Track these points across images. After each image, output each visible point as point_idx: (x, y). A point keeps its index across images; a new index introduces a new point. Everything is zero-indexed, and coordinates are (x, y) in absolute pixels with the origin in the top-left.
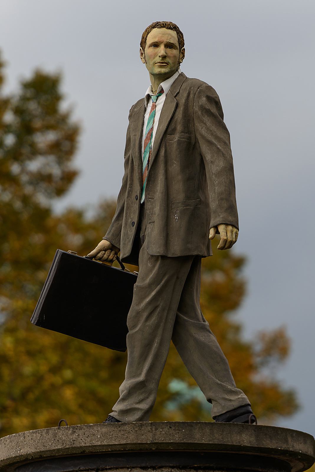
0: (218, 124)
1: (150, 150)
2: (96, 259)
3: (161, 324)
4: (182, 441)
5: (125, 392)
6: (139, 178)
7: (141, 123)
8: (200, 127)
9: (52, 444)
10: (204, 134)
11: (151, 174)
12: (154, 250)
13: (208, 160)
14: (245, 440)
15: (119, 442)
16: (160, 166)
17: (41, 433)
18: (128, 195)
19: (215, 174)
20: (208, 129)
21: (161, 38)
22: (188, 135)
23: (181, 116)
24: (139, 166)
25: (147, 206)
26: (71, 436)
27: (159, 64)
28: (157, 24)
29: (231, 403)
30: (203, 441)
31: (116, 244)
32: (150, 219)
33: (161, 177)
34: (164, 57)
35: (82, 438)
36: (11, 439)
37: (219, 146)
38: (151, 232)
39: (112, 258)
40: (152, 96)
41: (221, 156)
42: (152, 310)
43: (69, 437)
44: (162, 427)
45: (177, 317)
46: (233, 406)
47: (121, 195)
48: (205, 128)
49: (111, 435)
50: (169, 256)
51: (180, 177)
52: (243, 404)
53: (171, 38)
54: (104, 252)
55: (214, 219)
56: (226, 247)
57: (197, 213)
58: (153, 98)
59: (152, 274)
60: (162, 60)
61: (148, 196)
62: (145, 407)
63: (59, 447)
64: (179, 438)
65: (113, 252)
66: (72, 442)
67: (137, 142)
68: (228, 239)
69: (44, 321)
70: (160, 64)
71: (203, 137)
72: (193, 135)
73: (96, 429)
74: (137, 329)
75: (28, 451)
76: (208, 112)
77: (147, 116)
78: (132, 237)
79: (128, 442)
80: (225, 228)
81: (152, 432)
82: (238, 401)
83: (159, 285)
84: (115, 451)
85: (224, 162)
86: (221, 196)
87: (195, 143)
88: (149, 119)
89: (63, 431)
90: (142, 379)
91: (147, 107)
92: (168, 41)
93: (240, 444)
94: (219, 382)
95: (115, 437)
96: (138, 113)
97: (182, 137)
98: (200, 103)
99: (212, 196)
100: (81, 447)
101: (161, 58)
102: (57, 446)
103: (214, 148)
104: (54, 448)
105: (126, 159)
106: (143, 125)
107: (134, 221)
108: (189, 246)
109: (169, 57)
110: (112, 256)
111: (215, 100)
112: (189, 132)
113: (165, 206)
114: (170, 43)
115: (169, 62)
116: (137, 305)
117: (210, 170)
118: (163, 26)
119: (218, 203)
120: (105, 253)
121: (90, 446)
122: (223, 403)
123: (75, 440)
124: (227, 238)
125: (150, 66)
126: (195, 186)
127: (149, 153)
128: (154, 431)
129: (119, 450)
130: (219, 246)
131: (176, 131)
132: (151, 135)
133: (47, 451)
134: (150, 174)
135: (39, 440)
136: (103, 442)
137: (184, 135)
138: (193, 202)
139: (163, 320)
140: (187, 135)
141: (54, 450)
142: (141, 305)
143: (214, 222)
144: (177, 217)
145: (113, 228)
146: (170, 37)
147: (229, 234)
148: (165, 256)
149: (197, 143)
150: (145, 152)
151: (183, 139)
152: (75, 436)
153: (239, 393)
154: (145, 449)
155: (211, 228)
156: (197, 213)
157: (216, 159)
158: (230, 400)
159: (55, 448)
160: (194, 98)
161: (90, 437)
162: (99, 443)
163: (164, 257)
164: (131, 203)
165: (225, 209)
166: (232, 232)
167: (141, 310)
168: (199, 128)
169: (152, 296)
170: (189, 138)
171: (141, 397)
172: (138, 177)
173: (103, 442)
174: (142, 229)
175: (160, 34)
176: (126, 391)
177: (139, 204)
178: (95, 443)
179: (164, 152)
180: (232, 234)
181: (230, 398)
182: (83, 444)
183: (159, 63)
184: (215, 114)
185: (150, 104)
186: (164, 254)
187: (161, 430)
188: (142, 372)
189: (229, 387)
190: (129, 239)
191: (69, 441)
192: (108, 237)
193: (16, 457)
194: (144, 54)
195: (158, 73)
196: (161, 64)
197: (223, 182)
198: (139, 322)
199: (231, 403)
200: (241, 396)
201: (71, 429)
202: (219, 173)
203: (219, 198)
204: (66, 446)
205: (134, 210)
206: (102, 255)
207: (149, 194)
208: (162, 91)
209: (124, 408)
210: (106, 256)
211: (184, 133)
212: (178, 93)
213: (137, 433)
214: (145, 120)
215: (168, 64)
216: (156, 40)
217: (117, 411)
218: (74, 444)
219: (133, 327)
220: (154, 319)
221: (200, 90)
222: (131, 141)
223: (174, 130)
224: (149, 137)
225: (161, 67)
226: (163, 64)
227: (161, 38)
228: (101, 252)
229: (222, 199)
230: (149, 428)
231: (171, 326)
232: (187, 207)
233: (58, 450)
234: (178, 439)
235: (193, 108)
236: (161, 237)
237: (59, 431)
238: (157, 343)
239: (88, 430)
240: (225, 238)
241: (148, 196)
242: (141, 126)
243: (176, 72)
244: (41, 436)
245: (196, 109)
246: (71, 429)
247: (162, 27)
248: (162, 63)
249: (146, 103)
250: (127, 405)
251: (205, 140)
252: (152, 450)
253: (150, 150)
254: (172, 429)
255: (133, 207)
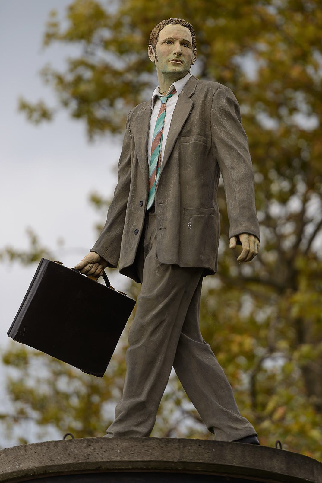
0: (238, 129)
1: (160, 152)
2: (82, 272)
3: (166, 341)
4: (212, 462)
5: (123, 412)
6: (146, 182)
7: (147, 126)
8: (219, 130)
9: (61, 459)
10: (224, 137)
11: (163, 177)
12: (166, 258)
13: (228, 165)
14: (276, 466)
15: (142, 459)
16: (172, 170)
17: (47, 446)
18: (131, 201)
19: (235, 180)
20: (227, 133)
21: (176, 35)
22: (205, 138)
23: (198, 118)
24: (146, 170)
25: (158, 211)
26: (85, 450)
27: (173, 62)
28: (172, 21)
29: (238, 432)
30: (235, 464)
31: (106, 257)
32: (161, 225)
33: (174, 181)
34: (180, 55)
35: (98, 452)
36: (7, 453)
37: (240, 152)
38: (162, 239)
39: (99, 272)
40: (161, 97)
41: (242, 162)
42: (158, 323)
43: (83, 450)
44: (191, 445)
45: (181, 337)
46: (240, 436)
47: (114, 205)
48: (224, 132)
49: (133, 450)
50: (182, 266)
51: (195, 182)
52: (251, 434)
53: (186, 36)
54: (92, 264)
55: (235, 227)
56: (247, 259)
57: (211, 223)
58: (163, 98)
59: (161, 285)
60: (177, 58)
61: (158, 200)
62: (144, 431)
63: (70, 461)
64: (209, 458)
65: (101, 266)
66: (87, 456)
67: (143, 145)
68: (251, 250)
69: (23, 335)
70: (174, 62)
71: (222, 141)
72: (209, 139)
73: (116, 443)
74: (141, 344)
75: (30, 465)
76: (228, 115)
77: (154, 118)
78: (135, 245)
79: (152, 460)
80: (248, 238)
81: (179, 450)
82: (245, 431)
83: (167, 296)
84: (137, 469)
85: (245, 169)
86: (243, 204)
87: (211, 148)
88: (157, 120)
89: (76, 443)
90: (143, 399)
91: (153, 109)
92: (184, 38)
93: (271, 471)
94: (224, 409)
95: (137, 453)
96: (141, 116)
97: (199, 139)
98: (220, 105)
99: (232, 204)
100: (97, 462)
101: (176, 56)
102: (67, 460)
103: (234, 153)
104: (64, 463)
105: (121, 167)
106: (149, 127)
107: (137, 229)
108: (202, 257)
109: (184, 55)
110: (100, 270)
111: (235, 103)
112: (206, 136)
113: (178, 211)
114: (186, 40)
115: (183, 61)
116: (142, 318)
117: (229, 177)
118: (178, 22)
119: (240, 212)
120: (93, 266)
121: (107, 461)
122: (229, 431)
123: (90, 455)
124: (250, 249)
125: (163, 64)
126: (209, 194)
127: (158, 156)
128: (182, 449)
129: (141, 469)
130: (240, 257)
131: (191, 134)
132: (161, 137)
133: (54, 466)
134: (162, 177)
135: (45, 453)
136: (124, 458)
137: (200, 138)
138: (207, 210)
139: (168, 337)
140: (203, 138)
141: (64, 465)
142: (146, 318)
143: (235, 231)
144: (190, 225)
145: (103, 240)
146: (186, 34)
147: (252, 245)
148: (177, 265)
149: (213, 148)
150: (153, 156)
151: (200, 142)
152: (89, 450)
153: (245, 422)
154: (170, 468)
155: (231, 237)
156: (211, 223)
157: (236, 165)
158: (237, 429)
159: (65, 463)
160: (212, 99)
161: (108, 452)
162: (119, 459)
163: (175, 267)
164: (134, 210)
165: (248, 217)
166: (254, 243)
167: (146, 323)
168: (218, 131)
169: (159, 308)
170: (205, 142)
171: (140, 419)
172: (145, 181)
173: (124, 458)
174: (145, 238)
175: (175, 30)
176: (124, 411)
177: (145, 210)
178: (114, 459)
179: (178, 155)
180: (254, 245)
181: (236, 427)
182: (100, 460)
183: (174, 60)
184: (235, 118)
185: (159, 104)
186: (177, 263)
187: (190, 448)
188: (143, 391)
189: (235, 415)
190: (132, 247)
191: (82, 455)
192: (97, 249)
193: (14, 472)
194: (155, 51)
195: (172, 71)
196: (176, 62)
197: (244, 189)
198: (143, 337)
199: (238, 432)
200: (248, 425)
201: (86, 442)
202: (240, 179)
203: (241, 206)
204: (78, 461)
205: (137, 218)
206: (89, 268)
207: (160, 199)
208: (174, 91)
209: (122, 430)
210: (93, 270)
211: (201, 136)
212: (194, 94)
213: (162, 450)
214: (151, 122)
215: (182, 63)
216: (171, 36)
217: (112, 433)
218: (88, 458)
219: (136, 341)
220: (159, 335)
221: (220, 91)
222: (135, 144)
223: (190, 132)
224: (159, 139)
225: (175, 65)
226: (177, 62)
227: (176, 35)
228: (89, 265)
229: (244, 207)
230: (176, 445)
231: (175, 344)
232: (202, 215)
233: (69, 465)
234: (208, 459)
235: (211, 110)
236: (174, 245)
237: (70, 443)
238: (160, 362)
239: (106, 443)
240: (248, 249)
241: (158, 200)
242: (146, 129)
243: (188, 73)
244: (48, 449)
245: (215, 110)
246: (86, 442)
247: (177, 23)
248: (177, 61)
249: (153, 105)
250: (124, 427)
251: (224, 144)
252: (179, 470)
253: (160, 152)
254: (201, 448)
255: (136, 213)
